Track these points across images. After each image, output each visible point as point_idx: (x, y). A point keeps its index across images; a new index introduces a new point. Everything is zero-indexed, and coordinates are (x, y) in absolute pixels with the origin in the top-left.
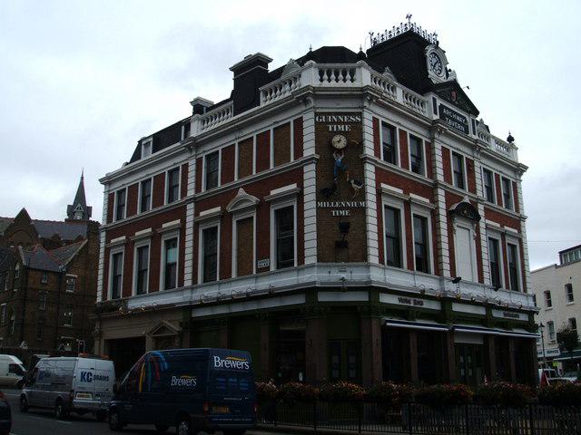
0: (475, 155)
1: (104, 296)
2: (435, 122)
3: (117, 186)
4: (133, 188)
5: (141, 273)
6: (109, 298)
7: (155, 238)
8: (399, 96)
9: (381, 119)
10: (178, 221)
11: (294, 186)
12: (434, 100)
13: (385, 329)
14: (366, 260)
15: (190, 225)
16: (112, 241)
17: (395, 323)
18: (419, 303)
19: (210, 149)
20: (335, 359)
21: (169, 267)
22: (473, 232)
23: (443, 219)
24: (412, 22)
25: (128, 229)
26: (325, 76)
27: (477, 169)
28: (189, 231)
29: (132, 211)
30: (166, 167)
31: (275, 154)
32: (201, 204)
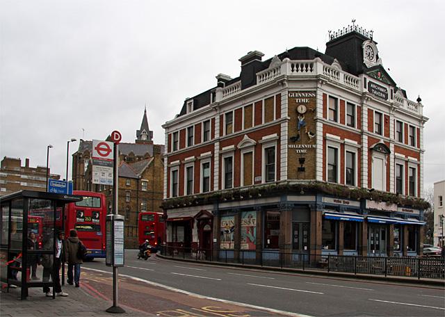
0: (391, 112)
1: (168, 196)
2: (364, 94)
3: (173, 130)
4: (183, 132)
5: (189, 182)
6: (171, 197)
7: (197, 162)
8: (341, 79)
9: (328, 94)
10: (210, 153)
11: (275, 135)
12: (365, 79)
13: (323, 217)
14: (315, 178)
15: (216, 155)
16: (171, 163)
17: (330, 214)
18: (346, 203)
19: (227, 109)
20: (296, 233)
21: (205, 179)
22: (385, 161)
23: (365, 153)
24: (356, 24)
25: (181, 156)
26: (295, 68)
27: (392, 122)
28: (216, 159)
29: (182, 146)
30: (202, 119)
31: (265, 115)
32: (223, 143)
